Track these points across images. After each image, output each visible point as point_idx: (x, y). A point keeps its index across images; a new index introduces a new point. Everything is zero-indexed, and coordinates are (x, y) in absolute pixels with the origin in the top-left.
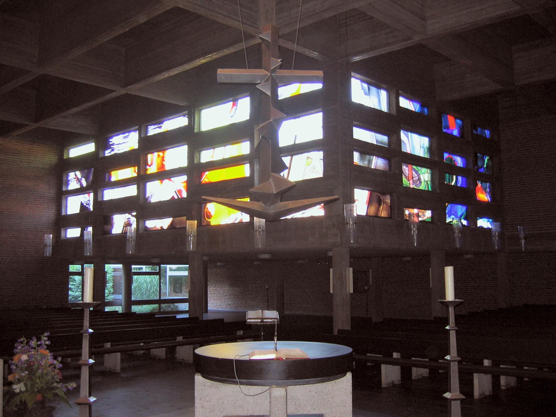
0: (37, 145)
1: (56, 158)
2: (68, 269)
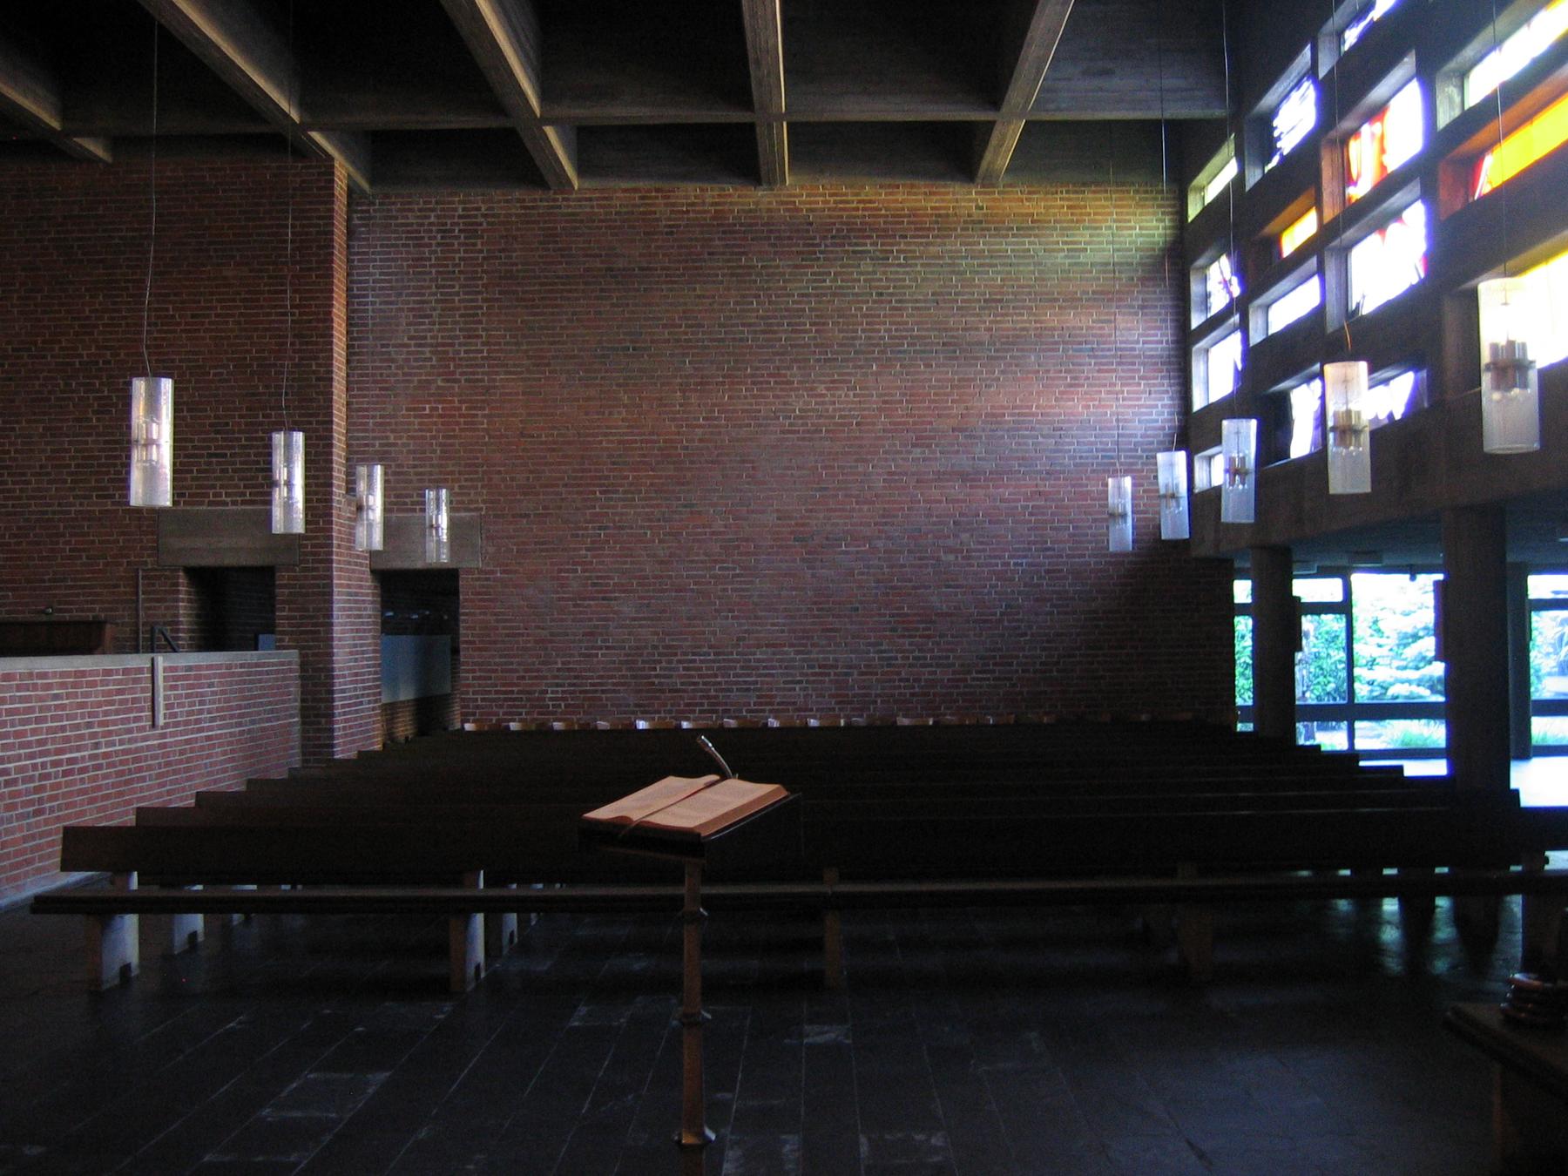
0: (1094, 192)
1: (1167, 402)
2: (1254, 589)
